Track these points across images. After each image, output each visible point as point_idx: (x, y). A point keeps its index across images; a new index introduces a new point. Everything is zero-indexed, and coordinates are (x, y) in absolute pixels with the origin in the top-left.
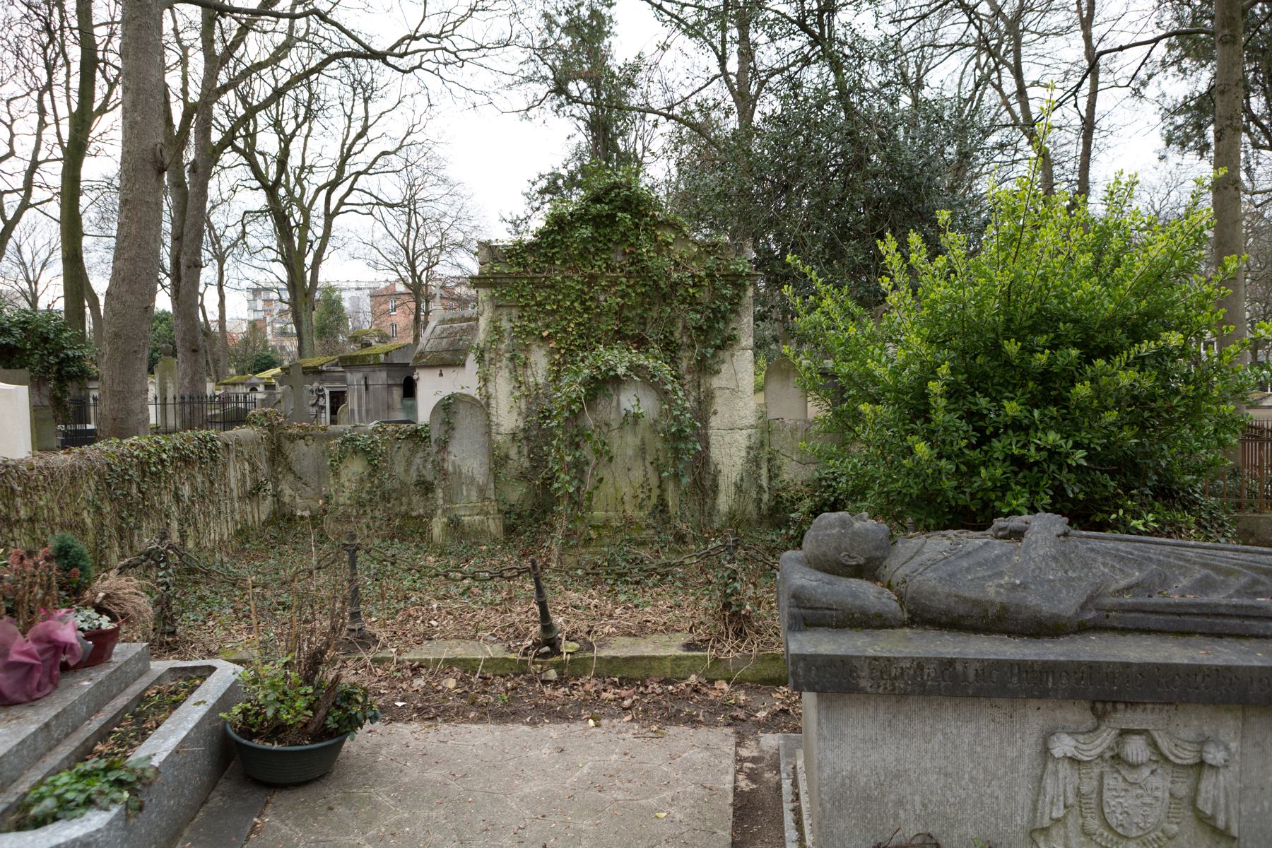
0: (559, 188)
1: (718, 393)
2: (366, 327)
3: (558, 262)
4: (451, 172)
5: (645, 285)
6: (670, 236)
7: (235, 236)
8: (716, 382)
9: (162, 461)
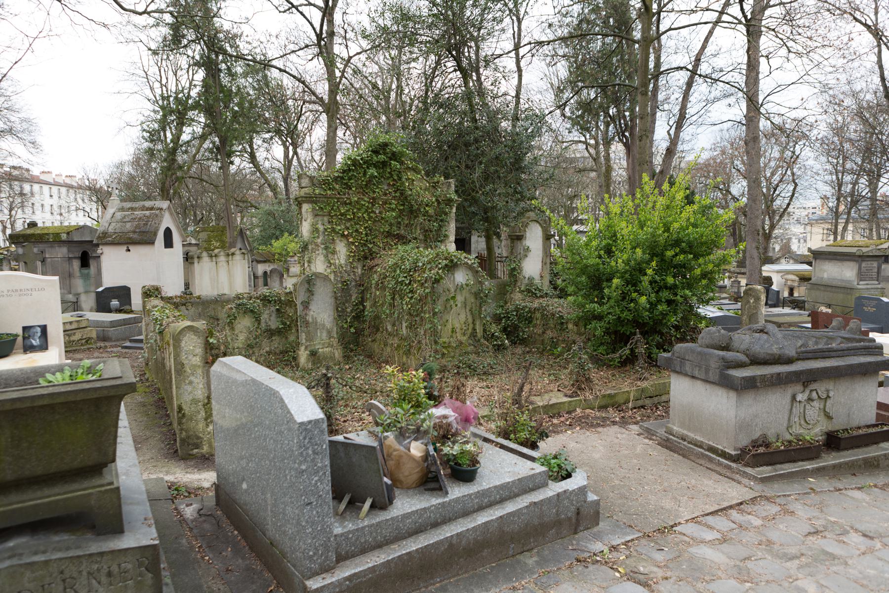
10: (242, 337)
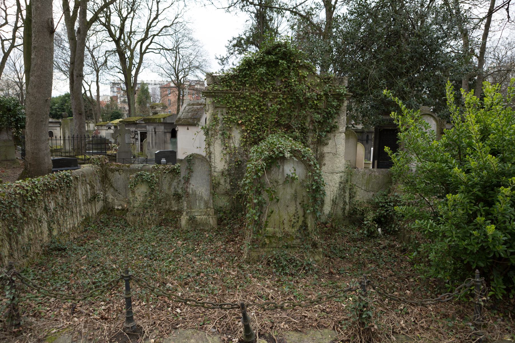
0: (242, 44)
1: (326, 155)
2: (157, 102)
3: (247, 85)
4: (195, 36)
5: (292, 99)
6: (306, 73)
7: (103, 61)
8: (326, 149)
9: (35, 194)
10: (140, 199)
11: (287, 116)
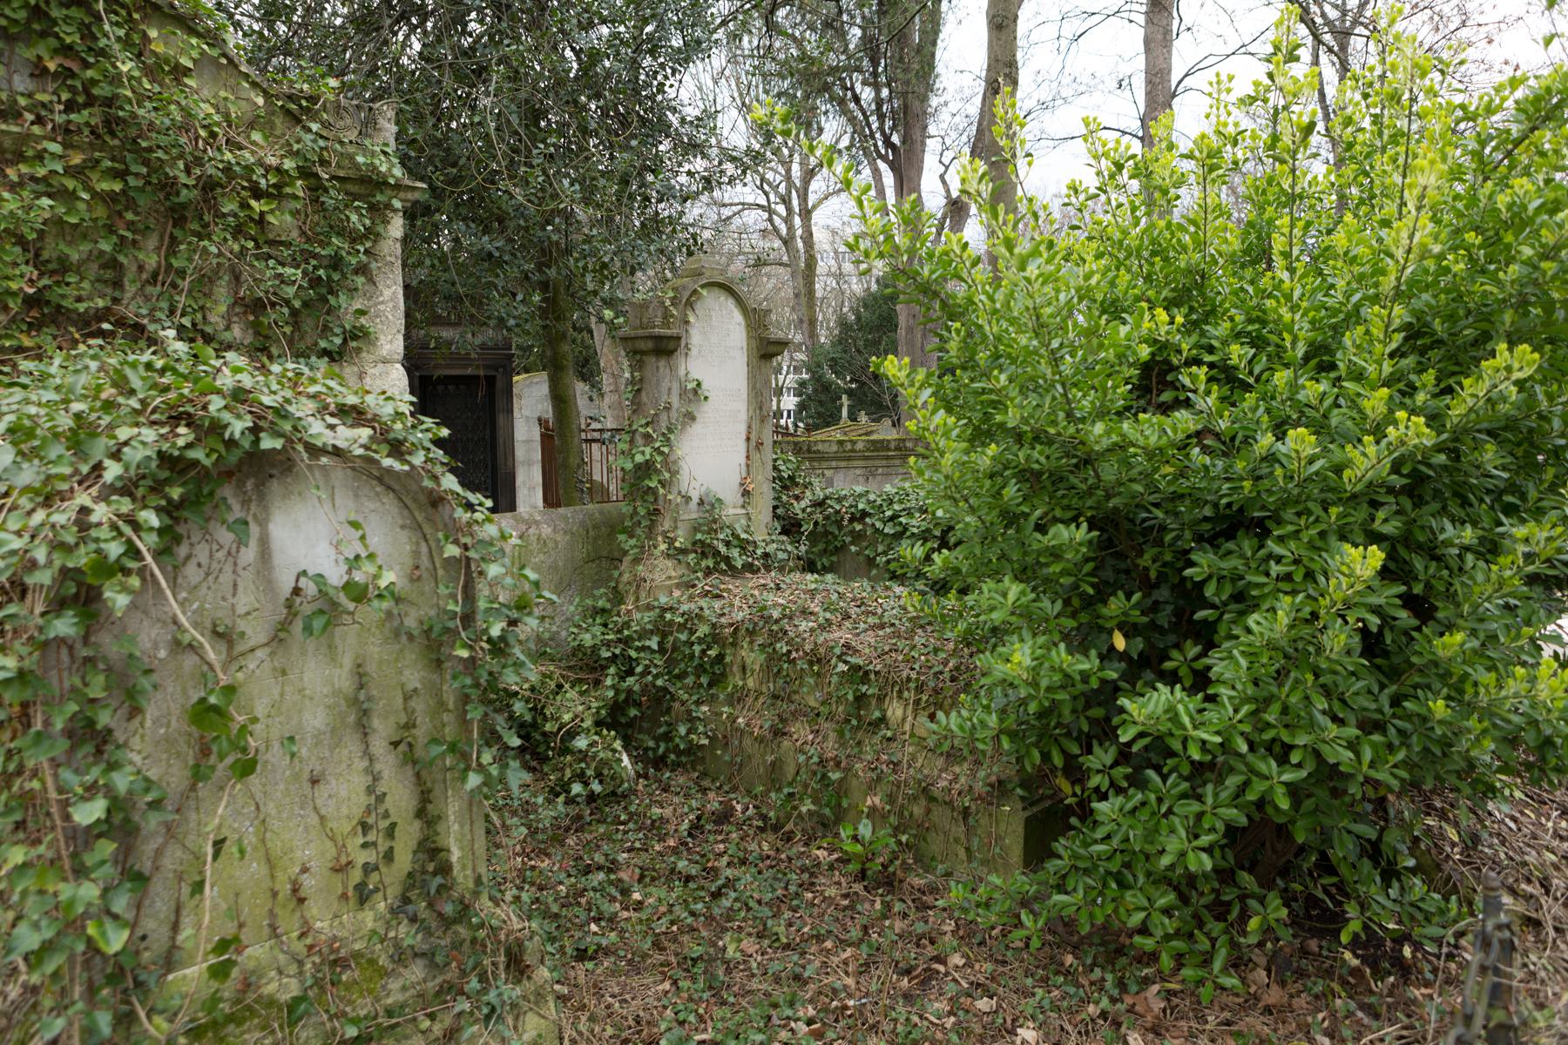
5: (121, 175)
11: (93, 270)
